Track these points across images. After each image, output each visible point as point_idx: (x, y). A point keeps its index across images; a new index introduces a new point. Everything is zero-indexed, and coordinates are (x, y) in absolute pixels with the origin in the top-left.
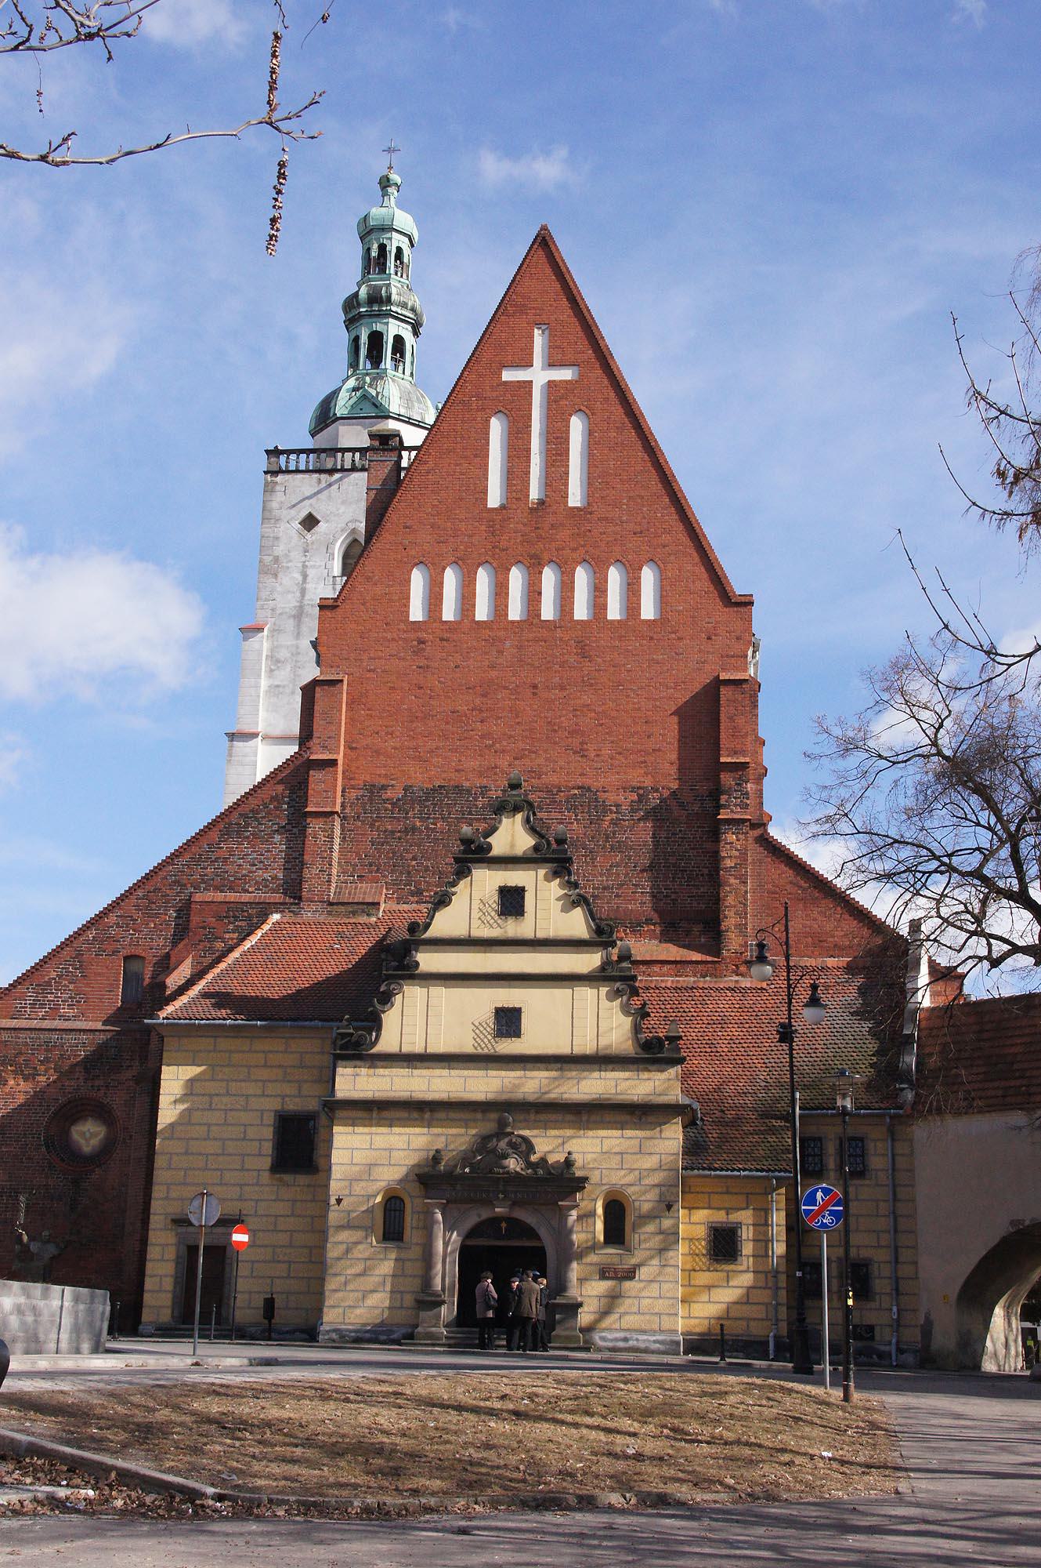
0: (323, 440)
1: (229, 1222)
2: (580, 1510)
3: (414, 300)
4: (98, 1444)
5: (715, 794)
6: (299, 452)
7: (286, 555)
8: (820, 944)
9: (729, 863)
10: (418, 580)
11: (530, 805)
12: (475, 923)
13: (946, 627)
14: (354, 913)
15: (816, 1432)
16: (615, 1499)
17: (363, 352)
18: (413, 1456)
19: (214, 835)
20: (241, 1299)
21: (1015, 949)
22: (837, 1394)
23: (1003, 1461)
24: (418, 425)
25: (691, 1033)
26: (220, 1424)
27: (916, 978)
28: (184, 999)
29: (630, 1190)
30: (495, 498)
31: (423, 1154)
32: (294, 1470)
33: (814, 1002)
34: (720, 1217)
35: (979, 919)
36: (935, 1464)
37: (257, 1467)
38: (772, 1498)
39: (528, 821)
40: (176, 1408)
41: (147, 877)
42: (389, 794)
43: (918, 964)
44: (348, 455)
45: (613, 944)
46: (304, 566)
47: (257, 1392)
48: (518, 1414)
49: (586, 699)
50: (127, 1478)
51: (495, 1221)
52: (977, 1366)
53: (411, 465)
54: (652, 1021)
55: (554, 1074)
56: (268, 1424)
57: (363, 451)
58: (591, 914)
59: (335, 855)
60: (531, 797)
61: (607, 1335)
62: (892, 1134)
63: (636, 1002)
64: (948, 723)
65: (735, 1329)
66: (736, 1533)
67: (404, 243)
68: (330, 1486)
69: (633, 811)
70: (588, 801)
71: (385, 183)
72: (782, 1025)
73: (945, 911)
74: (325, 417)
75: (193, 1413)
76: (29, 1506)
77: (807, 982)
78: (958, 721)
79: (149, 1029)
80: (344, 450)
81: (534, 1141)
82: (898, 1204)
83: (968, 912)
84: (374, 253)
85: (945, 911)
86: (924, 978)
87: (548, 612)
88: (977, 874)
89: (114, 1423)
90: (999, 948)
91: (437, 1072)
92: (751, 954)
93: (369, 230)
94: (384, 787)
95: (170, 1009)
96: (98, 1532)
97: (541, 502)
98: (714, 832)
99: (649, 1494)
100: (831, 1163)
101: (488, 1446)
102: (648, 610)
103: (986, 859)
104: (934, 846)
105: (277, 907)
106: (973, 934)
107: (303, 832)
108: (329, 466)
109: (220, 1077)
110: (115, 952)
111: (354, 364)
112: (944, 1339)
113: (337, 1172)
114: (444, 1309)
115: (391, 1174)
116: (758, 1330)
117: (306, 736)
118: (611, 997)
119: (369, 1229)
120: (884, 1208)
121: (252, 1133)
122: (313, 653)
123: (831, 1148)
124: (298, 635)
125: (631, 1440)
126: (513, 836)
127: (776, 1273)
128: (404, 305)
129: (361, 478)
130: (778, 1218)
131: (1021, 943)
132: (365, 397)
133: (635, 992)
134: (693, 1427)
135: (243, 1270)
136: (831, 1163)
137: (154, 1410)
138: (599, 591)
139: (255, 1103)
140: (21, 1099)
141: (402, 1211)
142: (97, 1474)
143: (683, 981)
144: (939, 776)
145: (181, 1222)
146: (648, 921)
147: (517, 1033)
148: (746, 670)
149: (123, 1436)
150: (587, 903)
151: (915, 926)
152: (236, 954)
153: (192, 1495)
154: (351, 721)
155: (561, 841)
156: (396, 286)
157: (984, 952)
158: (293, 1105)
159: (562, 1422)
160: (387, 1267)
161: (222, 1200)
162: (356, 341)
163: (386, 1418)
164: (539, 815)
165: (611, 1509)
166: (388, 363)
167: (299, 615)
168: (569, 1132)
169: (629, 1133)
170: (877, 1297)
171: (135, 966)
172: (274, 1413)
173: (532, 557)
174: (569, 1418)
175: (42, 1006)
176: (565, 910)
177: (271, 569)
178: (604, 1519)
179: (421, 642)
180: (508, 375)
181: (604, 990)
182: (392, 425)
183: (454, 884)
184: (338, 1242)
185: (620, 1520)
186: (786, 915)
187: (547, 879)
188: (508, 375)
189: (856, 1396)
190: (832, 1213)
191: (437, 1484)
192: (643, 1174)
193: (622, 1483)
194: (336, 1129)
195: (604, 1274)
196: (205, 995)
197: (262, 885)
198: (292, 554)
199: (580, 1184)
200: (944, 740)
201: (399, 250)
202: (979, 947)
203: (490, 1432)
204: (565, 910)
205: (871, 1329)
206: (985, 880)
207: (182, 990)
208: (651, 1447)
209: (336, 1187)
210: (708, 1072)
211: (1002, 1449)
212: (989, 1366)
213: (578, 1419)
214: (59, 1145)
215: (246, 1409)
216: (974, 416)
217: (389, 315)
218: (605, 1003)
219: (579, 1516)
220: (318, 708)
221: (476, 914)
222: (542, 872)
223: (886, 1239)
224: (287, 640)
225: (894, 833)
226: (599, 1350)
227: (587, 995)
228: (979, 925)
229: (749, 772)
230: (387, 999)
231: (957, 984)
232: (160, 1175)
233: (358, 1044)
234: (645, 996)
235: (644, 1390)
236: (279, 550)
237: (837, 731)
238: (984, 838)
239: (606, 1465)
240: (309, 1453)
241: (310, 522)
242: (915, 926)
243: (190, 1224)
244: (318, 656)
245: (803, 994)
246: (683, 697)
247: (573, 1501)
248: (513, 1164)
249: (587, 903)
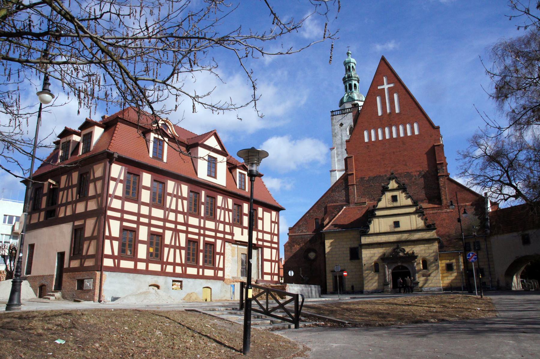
0: (342, 107)
1: (343, 271)
2: (425, 323)
3: (357, 76)
4: (323, 314)
5: (437, 170)
6: (337, 111)
7: (338, 132)
8: (465, 200)
9: (441, 185)
10: (366, 133)
11: (396, 177)
12: (387, 204)
13: (488, 124)
14: (361, 205)
15: (476, 305)
16: (432, 320)
17: (348, 88)
18: (388, 314)
20: (347, 286)
21: (510, 196)
22: (479, 297)
23: (521, 308)
24: (362, 101)
25: (437, 223)
26: (348, 310)
27: (487, 206)
28: (328, 226)
29: (427, 258)
30: (380, 114)
31: (381, 254)
32: (363, 318)
33: (465, 213)
34: (448, 262)
35: (501, 191)
36: (504, 309)
37: (355, 318)
38: (467, 318)
39: (396, 181)
40: (337, 307)
41: (317, 202)
42: (365, 179)
43: (487, 203)
44: (348, 110)
45: (418, 205)
47: (354, 303)
48: (408, 305)
49: (405, 153)
50: (330, 320)
51: (399, 266)
52: (511, 289)
53: (361, 110)
54: (428, 221)
55: (408, 234)
56: (357, 309)
57: (350, 108)
58: (412, 199)
59: (356, 193)
60: (396, 176)
61: (425, 289)
62: (486, 240)
63: (424, 217)
64: (488, 148)
65: (453, 285)
66: (461, 326)
67: (353, 65)
68: (371, 321)
69: (419, 176)
70: (408, 175)
71: (348, 54)
72: (458, 219)
73: (492, 190)
74: (342, 103)
75: (341, 308)
76: (312, 326)
77: (463, 209)
78: (490, 147)
79: (322, 233)
80: (347, 109)
81: (405, 249)
83: (498, 189)
84: (348, 68)
85: (492, 190)
86: (489, 205)
87: (394, 136)
88: (499, 180)
89: (326, 310)
90: (506, 197)
91: (383, 236)
92: (449, 204)
93: (347, 64)
94: (364, 178)
95: (325, 228)
96: (326, 330)
97: (390, 113)
98: (437, 178)
99: (440, 319)
100: (472, 247)
101: (403, 311)
102: (416, 133)
103: (501, 177)
104: (488, 176)
105: (345, 205)
106: (499, 194)
107: (348, 189)
108: (344, 112)
110: (313, 218)
111: (346, 91)
112: (502, 284)
113: (364, 259)
114: (389, 285)
115: (375, 258)
116: (459, 285)
117: (346, 169)
118: (419, 216)
119: (372, 270)
122: (346, 152)
123: (472, 245)
124: (342, 148)
125: (434, 309)
127: (462, 273)
128: (355, 77)
129: (351, 114)
130: (461, 260)
131: (511, 195)
132: (350, 97)
133: (424, 215)
134: (448, 305)
135: (346, 280)
136: (472, 247)
137: (333, 307)
140: (298, 249)
141: (378, 265)
142: (324, 320)
143: (434, 211)
144: (488, 161)
145: (333, 271)
146: (425, 200)
147: (399, 227)
148: (440, 142)
149: (328, 312)
150: (411, 197)
151: (486, 194)
152: (337, 216)
153: (343, 323)
154: (355, 165)
155: (404, 184)
156: (353, 73)
157: (503, 198)
158: (353, 246)
159: (419, 306)
160: (377, 278)
161: (341, 266)
162: (346, 86)
163: (381, 307)
164: (399, 179)
165: (432, 322)
166: (353, 89)
167: (342, 144)
168: (413, 246)
169: (426, 245)
171: (317, 220)
172: (358, 307)
174: (420, 305)
176: (406, 199)
177: (334, 135)
178: (431, 324)
179: (368, 146)
180: (379, 88)
181: (417, 215)
182: (356, 102)
183: (382, 196)
184: (366, 273)
185: (434, 325)
186: (456, 194)
187: (402, 193)
188: (379, 88)
189: (484, 297)
190: (474, 258)
191: (393, 319)
192: (430, 253)
193: (433, 317)
194: (362, 250)
195: (423, 276)
196: (332, 225)
197: (341, 201)
199: (416, 257)
200: (488, 152)
201: (353, 66)
202: (502, 197)
203: (403, 309)
204: (406, 199)
206: (501, 182)
207: (327, 224)
208: (439, 310)
209: (364, 262)
210: (443, 231)
211: (520, 305)
212: (513, 289)
213: (422, 305)
214: (306, 257)
215: (352, 306)
216: (488, 77)
217: (352, 80)
218: (417, 218)
219: (425, 324)
220: (348, 163)
221: (387, 202)
222: (400, 192)
224: (340, 150)
225: (478, 174)
226: (424, 291)
227: (413, 217)
228: (501, 192)
229: (444, 164)
230: (370, 222)
231: (497, 206)
232: (327, 262)
233: (365, 232)
234: (426, 216)
235: (437, 299)
236: (336, 131)
237: (462, 153)
238: (500, 173)
239: (429, 314)
240: (366, 314)
241: (341, 125)
242: (486, 194)
243: (335, 271)
244: (347, 152)
245: (462, 211)
246: (427, 150)
247: (423, 321)
248: (401, 254)
249: (411, 197)
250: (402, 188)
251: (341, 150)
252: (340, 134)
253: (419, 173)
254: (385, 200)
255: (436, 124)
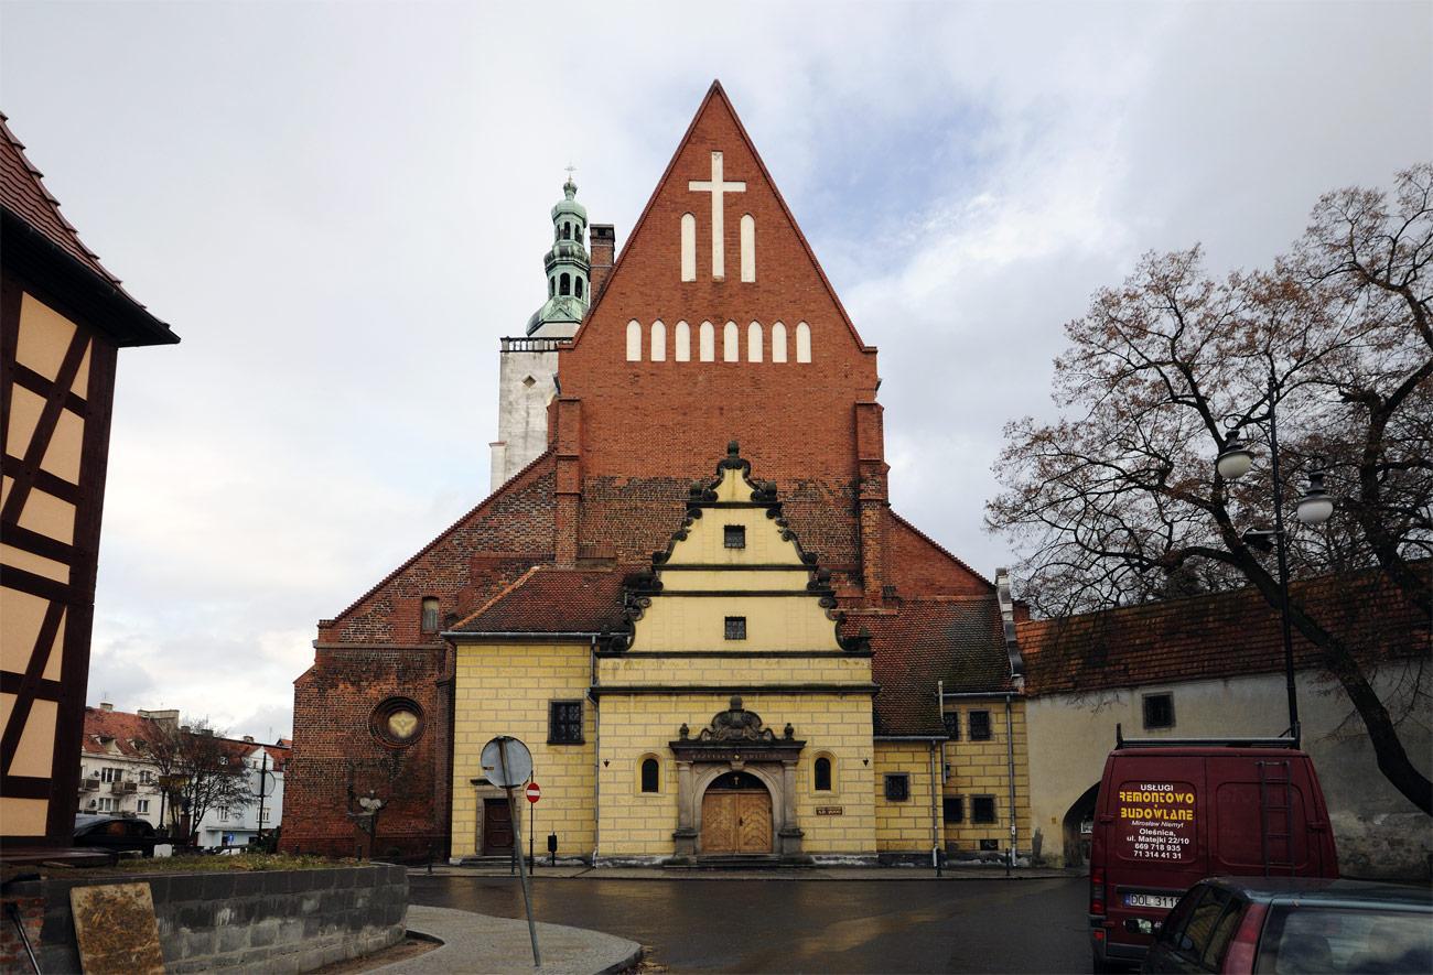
9: (867, 530)
10: (634, 331)
14: (595, 565)
19: (488, 510)
30: (688, 272)
41: (438, 541)
42: (617, 483)
46: (528, 408)
58: (799, 548)
82: (1015, 757)
84: (562, 228)
109: (503, 675)
120: (1004, 760)
121: (530, 716)
126: (734, 487)
138: (767, 341)
139: (531, 694)
158: (564, 695)
170: (912, 798)
173: (715, 317)
175: (362, 633)
183: (689, 523)
198: (520, 401)
201: (577, 227)
205: (996, 841)
223: (1005, 781)
232: (457, 748)
236: (511, 398)
241: (530, 381)
250: (766, 499)
251: (522, 452)
252: (523, 403)
253: (796, 486)
254: (704, 538)
255: (867, 343)
